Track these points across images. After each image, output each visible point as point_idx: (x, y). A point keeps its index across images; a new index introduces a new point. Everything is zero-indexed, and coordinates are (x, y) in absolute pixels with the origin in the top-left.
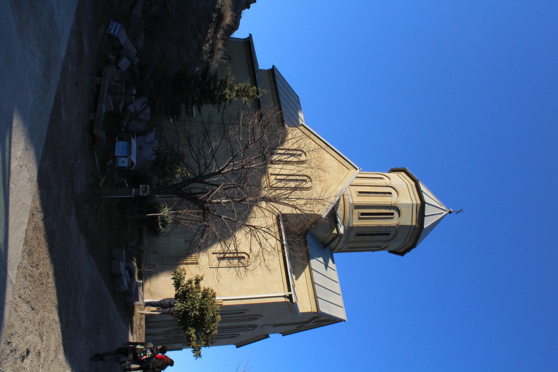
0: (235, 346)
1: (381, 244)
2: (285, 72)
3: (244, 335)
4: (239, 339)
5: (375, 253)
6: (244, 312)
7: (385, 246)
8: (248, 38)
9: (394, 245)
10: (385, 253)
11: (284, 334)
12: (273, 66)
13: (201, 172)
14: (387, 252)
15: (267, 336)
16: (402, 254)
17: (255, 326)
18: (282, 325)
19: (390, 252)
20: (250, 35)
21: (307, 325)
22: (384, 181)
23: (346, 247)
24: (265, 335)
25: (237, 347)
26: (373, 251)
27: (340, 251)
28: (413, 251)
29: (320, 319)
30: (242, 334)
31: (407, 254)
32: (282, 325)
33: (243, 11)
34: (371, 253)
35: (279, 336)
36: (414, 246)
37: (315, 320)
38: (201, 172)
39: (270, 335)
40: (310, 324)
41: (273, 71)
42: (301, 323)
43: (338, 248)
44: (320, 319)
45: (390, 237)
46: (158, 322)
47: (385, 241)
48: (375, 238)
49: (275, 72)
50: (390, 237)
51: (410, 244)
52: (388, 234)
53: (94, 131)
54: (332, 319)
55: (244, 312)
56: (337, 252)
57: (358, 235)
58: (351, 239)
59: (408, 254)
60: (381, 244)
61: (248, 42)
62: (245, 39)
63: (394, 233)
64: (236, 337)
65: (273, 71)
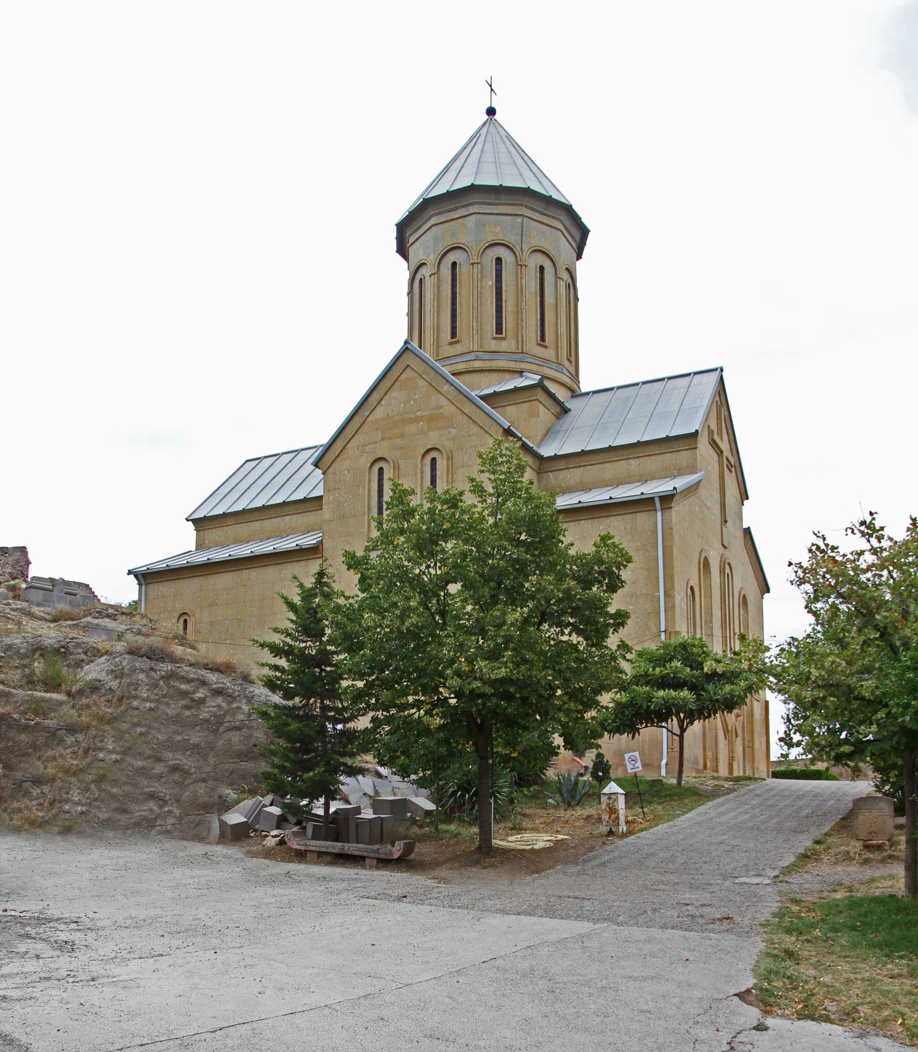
0: (766, 596)
2: (195, 495)
3: (743, 579)
4: (752, 589)
6: (692, 588)
7: (565, 276)
8: (136, 576)
9: (563, 248)
10: (582, 268)
11: (744, 495)
15: (747, 532)
16: (584, 232)
23: (566, 363)
25: (768, 591)
26: (577, 299)
27: (576, 376)
29: (714, 427)
30: (737, 585)
33: (103, 600)
36: (568, 209)
40: (724, 445)
41: (200, 523)
43: (568, 381)
44: (714, 427)
45: (547, 264)
48: (549, 299)
51: (563, 217)
52: (542, 269)
53: (396, 857)
54: (718, 399)
55: (692, 588)
56: (578, 382)
57: (543, 338)
58: (550, 354)
59: (585, 220)
62: (140, 584)
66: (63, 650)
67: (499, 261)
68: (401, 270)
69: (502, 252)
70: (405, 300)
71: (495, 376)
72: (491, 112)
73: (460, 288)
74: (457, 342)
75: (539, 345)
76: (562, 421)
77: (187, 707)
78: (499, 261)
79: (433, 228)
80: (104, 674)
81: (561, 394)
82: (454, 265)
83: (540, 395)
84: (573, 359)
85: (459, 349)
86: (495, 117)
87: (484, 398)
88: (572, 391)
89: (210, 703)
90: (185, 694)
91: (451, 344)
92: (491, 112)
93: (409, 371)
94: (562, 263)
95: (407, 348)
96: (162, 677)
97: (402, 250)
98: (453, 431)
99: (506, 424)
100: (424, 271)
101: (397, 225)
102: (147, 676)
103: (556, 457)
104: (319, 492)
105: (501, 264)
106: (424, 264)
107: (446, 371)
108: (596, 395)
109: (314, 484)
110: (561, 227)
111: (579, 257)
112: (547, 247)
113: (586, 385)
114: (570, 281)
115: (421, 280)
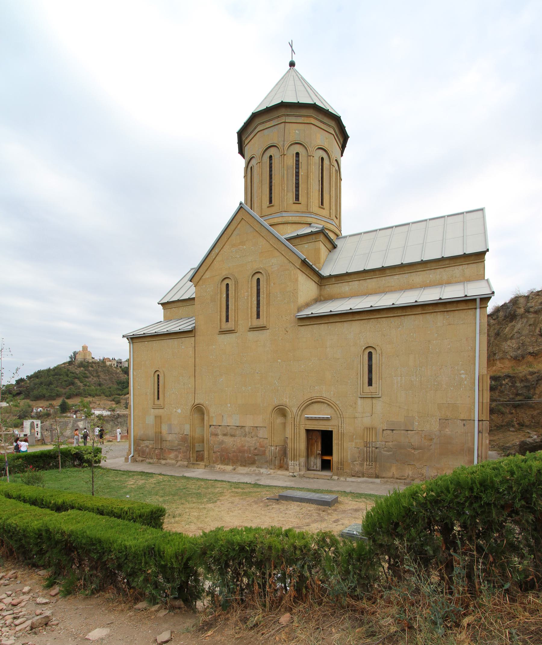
9: (335, 149)
23: (335, 219)
27: (339, 227)
36: (337, 120)
52: (322, 159)
56: (340, 231)
57: (322, 204)
67: (297, 154)
68: (241, 162)
69: (298, 148)
70: (243, 180)
71: (294, 226)
72: (292, 64)
73: (275, 175)
74: (273, 206)
75: (320, 207)
76: (332, 253)
78: (297, 154)
79: (258, 134)
81: (332, 236)
82: (271, 157)
83: (322, 237)
84: (338, 217)
85: (273, 210)
86: (295, 67)
87: (289, 239)
88: (337, 236)
91: (268, 207)
92: (292, 64)
93: (243, 222)
94: (333, 157)
95: (241, 207)
97: (241, 152)
99: (303, 257)
100: (253, 162)
101: (237, 133)
103: (330, 277)
104: (194, 296)
105: (299, 157)
106: (253, 157)
107: (266, 224)
108: (397, 228)
109: (190, 291)
110: (334, 133)
111: (342, 156)
112: (326, 146)
113: (344, 233)
114: (337, 168)
115: (251, 167)
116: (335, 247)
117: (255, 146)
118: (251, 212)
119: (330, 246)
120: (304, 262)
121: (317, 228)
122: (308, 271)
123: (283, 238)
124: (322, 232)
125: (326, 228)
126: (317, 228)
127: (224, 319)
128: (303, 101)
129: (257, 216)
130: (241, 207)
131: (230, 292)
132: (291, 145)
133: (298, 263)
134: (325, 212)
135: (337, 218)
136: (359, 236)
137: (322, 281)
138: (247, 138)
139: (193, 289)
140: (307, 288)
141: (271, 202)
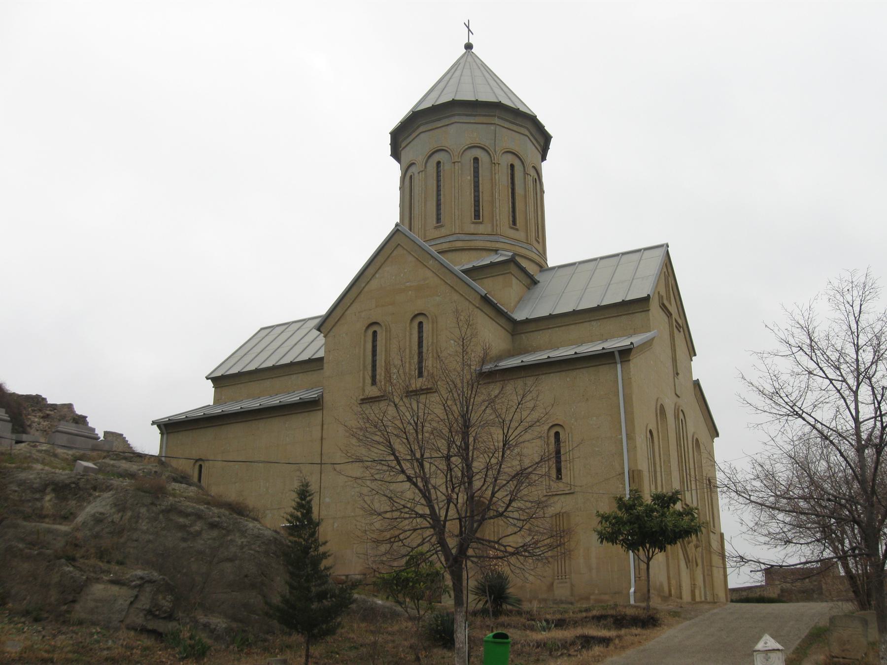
0: (716, 439)
1: (530, 180)
3: (694, 425)
4: (703, 435)
5: (545, 188)
6: (651, 432)
7: (533, 173)
8: (159, 426)
10: (546, 167)
11: (692, 352)
12: (207, 378)
13: (428, 525)
14: (544, 164)
15: (697, 384)
17: (679, 412)
18: (674, 360)
19: (544, 158)
20: (154, 423)
21: (675, 315)
22: (416, 174)
24: (695, 388)
25: (717, 435)
26: (542, 192)
27: (543, 254)
28: (540, 118)
29: (663, 293)
30: (691, 429)
31: (548, 128)
32: (674, 360)
34: (545, 196)
35: (696, 362)
37: (666, 302)
38: (428, 525)
39: (694, 378)
40: (673, 309)
42: (671, 325)
44: (663, 293)
45: (517, 163)
46: (669, 578)
47: (526, 173)
48: (519, 190)
49: (218, 374)
50: (517, 163)
51: (529, 125)
52: (512, 166)
54: (665, 270)
55: (651, 432)
57: (514, 223)
58: (521, 235)
60: (530, 180)
61: (169, 427)
62: (162, 434)
63: (510, 156)
64: (697, 440)
65: (219, 381)
66: (73, 486)
67: (476, 160)
68: (394, 169)
69: (479, 153)
72: (469, 47)
74: (442, 226)
75: (511, 228)
77: (184, 540)
78: (476, 160)
80: (108, 508)
81: (531, 268)
82: (439, 163)
83: (513, 268)
84: (540, 241)
87: (465, 272)
88: (541, 267)
89: (205, 536)
90: (182, 527)
91: (436, 228)
92: (469, 47)
96: (163, 511)
98: (437, 298)
99: (483, 292)
100: (413, 169)
102: (148, 511)
103: (527, 321)
104: (321, 354)
107: (433, 250)
110: (529, 134)
115: (411, 177)
116: (535, 282)
117: (416, 149)
118: (412, 235)
119: (529, 281)
120: (485, 299)
121: (505, 255)
122: (488, 309)
123: (457, 268)
124: (512, 261)
125: (519, 255)
126: (505, 255)
127: (369, 381)
128: (483, 98)
129: (420, 241)
130: (398, 230)
131: (378, 343)
132: (470, 148)
133: (477, 302)
134: (521, 235)
135: (539, 242)
136: (572, 267)
137: (516, 328)
138: (405, 139)
139: (321, 340)
140: (491, 336)
141: (438, 220)
